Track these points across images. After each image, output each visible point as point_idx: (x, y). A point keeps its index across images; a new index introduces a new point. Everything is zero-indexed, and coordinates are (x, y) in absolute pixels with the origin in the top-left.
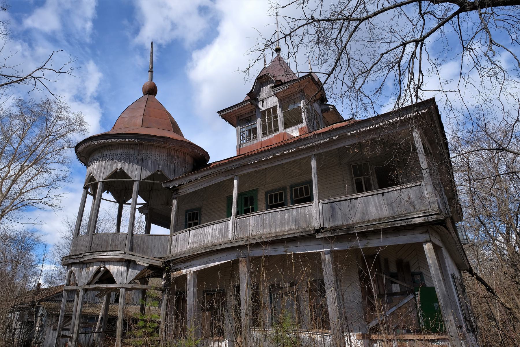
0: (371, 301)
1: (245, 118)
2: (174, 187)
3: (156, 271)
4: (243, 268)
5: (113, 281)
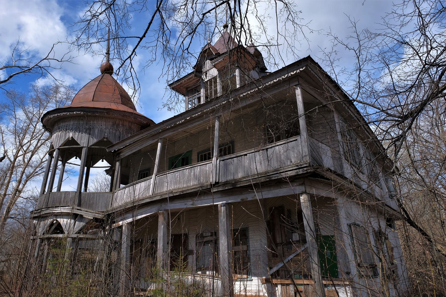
1: (192, 89)
2: (115, 151)
3: (98, 223)
4: (161, 219)
5: (62, 232)
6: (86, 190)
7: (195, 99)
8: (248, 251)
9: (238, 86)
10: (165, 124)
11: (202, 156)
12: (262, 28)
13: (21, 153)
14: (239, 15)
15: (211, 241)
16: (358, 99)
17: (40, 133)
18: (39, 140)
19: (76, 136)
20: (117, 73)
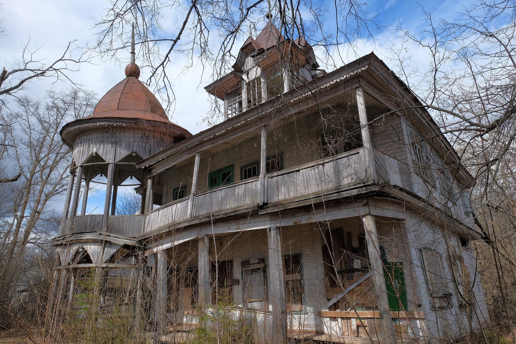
0: (333, 277)
2: (145, 167)
5: (89, 261)
6: (113, 213)
7: (235, 104)
8: (302, 281)
9: (286, 90)
10: (202, 136)
11: (245, 171)
12: (317, 23)
13: (38, 168)
14: (290, 7)
15: (259, 269)
16: (433, 105)
17: (59, 145)
18: (58, 154)
19: (101, 151)
20: (148, 83)
